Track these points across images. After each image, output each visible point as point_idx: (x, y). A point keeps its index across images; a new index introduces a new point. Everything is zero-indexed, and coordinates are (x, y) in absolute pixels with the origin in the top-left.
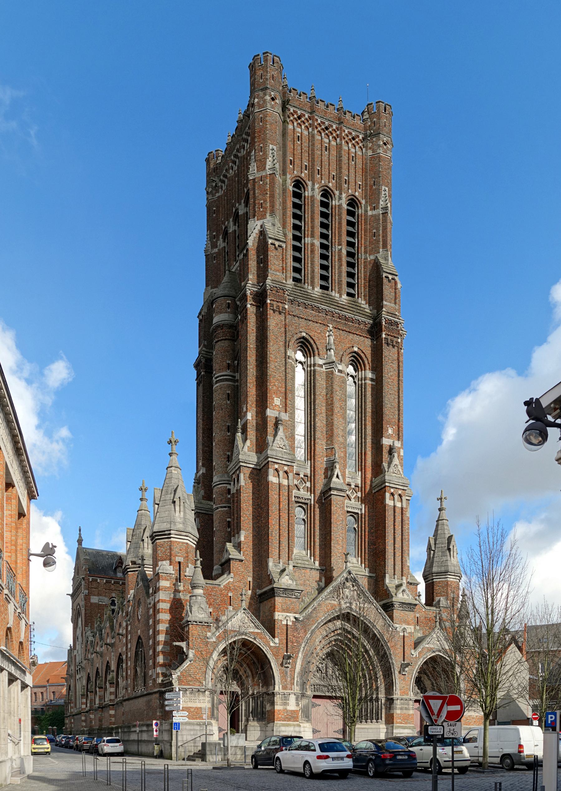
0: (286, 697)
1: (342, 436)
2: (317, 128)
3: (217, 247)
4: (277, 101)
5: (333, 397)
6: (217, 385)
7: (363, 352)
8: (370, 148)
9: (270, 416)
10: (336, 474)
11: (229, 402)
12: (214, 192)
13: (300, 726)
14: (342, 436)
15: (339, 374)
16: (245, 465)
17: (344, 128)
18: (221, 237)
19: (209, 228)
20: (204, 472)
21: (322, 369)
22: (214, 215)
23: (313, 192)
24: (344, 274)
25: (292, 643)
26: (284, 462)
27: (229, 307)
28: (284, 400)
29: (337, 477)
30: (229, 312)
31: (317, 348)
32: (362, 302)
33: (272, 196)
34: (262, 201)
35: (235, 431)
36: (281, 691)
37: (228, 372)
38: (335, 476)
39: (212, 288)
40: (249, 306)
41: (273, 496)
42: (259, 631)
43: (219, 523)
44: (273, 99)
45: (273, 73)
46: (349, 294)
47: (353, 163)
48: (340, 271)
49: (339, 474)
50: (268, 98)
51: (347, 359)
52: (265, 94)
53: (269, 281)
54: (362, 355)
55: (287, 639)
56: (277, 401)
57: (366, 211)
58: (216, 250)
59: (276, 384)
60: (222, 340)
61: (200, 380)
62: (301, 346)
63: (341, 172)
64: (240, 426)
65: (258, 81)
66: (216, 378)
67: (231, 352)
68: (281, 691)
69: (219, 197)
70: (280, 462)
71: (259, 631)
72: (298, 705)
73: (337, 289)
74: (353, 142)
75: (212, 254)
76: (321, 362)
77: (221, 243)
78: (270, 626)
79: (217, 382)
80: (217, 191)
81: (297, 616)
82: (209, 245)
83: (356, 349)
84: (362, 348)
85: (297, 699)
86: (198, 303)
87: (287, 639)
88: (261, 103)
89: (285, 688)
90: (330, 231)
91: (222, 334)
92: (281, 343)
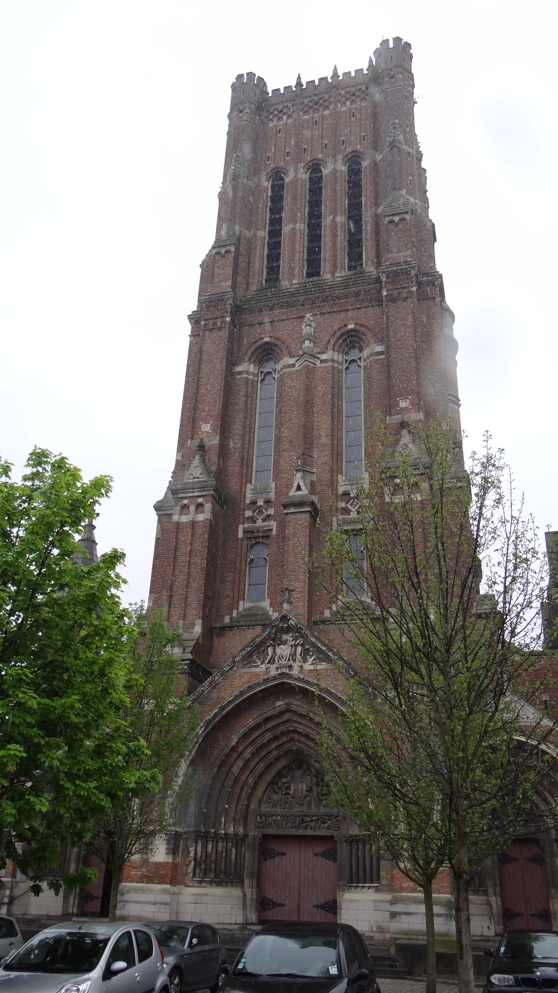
7: (364, 326)
15: (323, 365)
21: (293, 369)
49: (302, 484)
70: (190, 495)
76: (292, 361)
83: (351, 326)
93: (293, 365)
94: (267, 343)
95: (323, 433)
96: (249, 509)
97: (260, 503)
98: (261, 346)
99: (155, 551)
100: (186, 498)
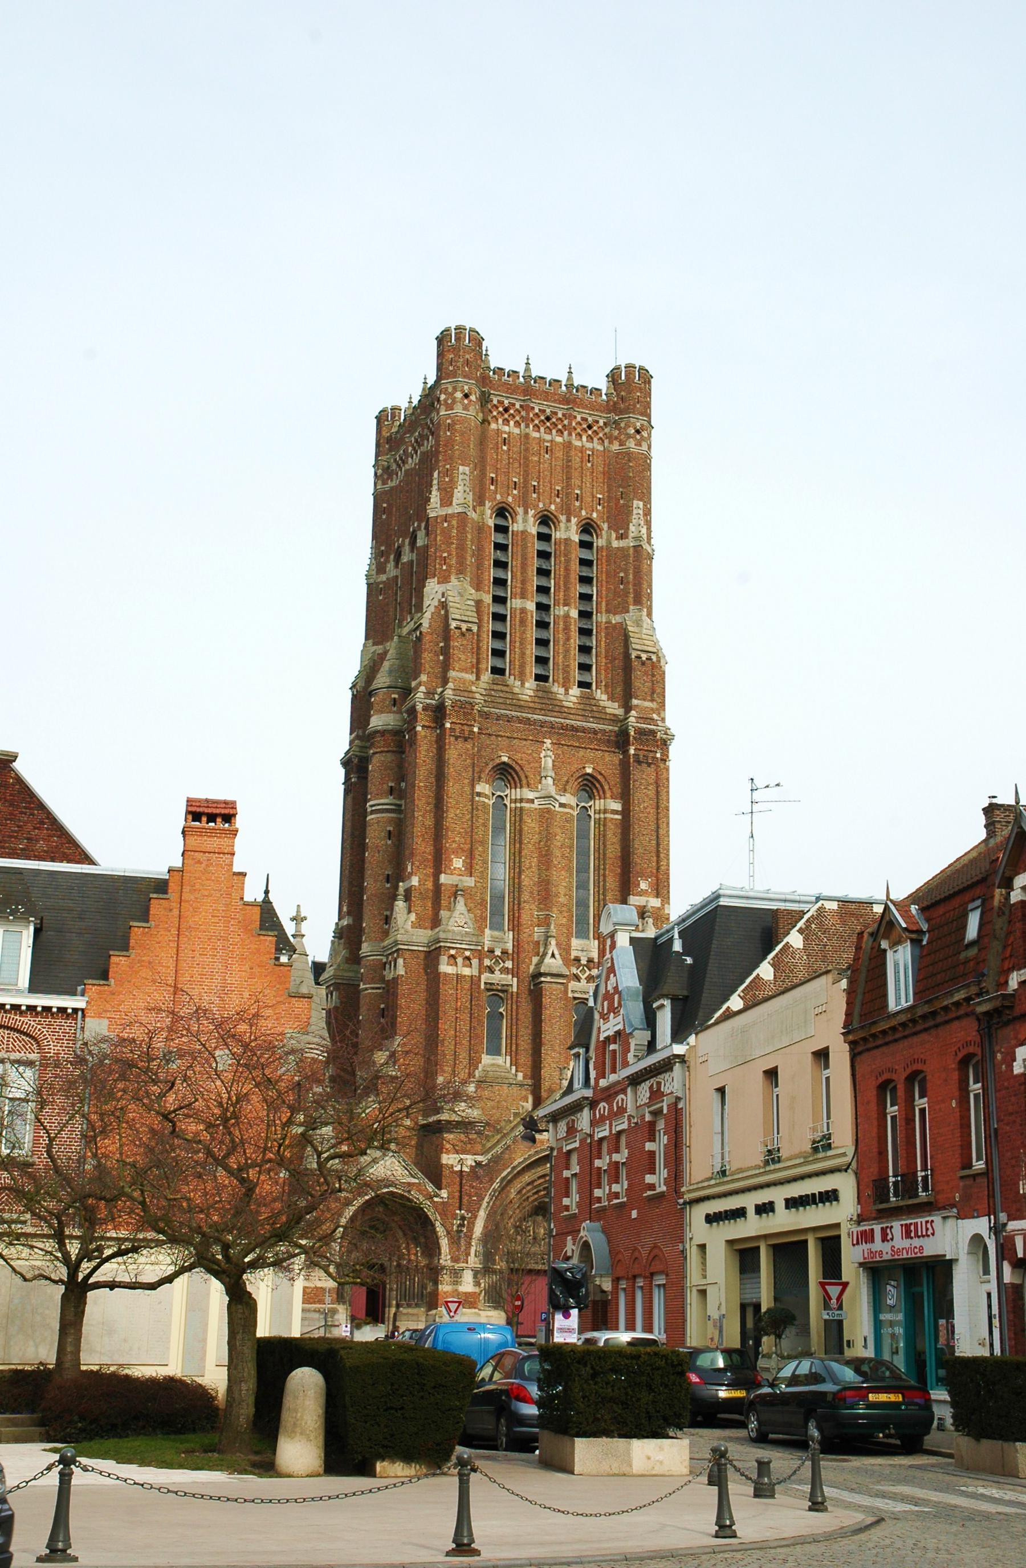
0: (456, 1275)
1: (565, 895)
2: (533, 421)
3: (385, 572)
4: (473, 398)
5: (549, 846)
6: (373, 816)
7: (601, 774)
8: (616, 438)
9: (446, 885)
10: (550, 952)
11: (389, 842)
12: (385, 477)
13: (479, 1315)
14: (565, 895)
15: (562, 809)
16: (406, 947)
17: (575, 414)
18: (392, 557)
19: (375, 537)
20: (351, 922)
21: (532, 806)
22: (384, 517)
23: (525, 523)
24: (574, 651)
25: (470, 1196)
26: (463, 946)
27: (394, 705)
28: (468, 861)
29: (553, 955)
30: (394, 712)
31: (526, 777)
32: (601, 696)
33: (461, 548)
34: (445, 555)
35: (394, 898)
36: (449, 1263)
37: (390, 800)
38: (550, 954)
39: (374, 644)
40: (419, 728)
41: (447, 991)
42: (417, 1181)
43: (368, 1010)
44: (466, 396)
45: (467, 356)
46: (582, 685)
47: (589, 465)
48: (565, 650)
49: (556, 952)
50: (459, 395)
51: (573, 785)
52: (455, 389)
53: (451, 692)
54: (599, 777)
55: (461, 1192)
56: (458, 863)
57: (609, 542)
58: (383, 578)
59: (457, 839)
60: (382, 752)
61: (349, 788)
62: (501, 774)
63: (569, 485)
64: (401, 891)
65: (447, 369)
66: (372, 806)
67: (396, 769)
68: (449, 1263)
69: (392, 488)
70: (458, 946)
71: (417, 1181)
72: (477, 1284)
73: (561, 681)
74: (590, 432)
75: (378, 584)
76: (531, 795)
77: (392, 571)
78: (435, 1173)
79: (372, 812)
80: (390, 477)
81: (479, 1158)
82: (374, 567)
83: (589, 770)
84: (599, 768)
85: (475, 1276)
86: (351, 667)
87: (461, 1192)
88: (449, 402)
89: (455, 1259)
90: (552, 582)
91: (382, 743)
92: (466, 781)
93: (532, 801)
94: (504, 763)
95: (562, 891)
96: (487, 957)
97: (498, 953)
98: (499, 764)
99: (42, 806)
100: (453, 948)
